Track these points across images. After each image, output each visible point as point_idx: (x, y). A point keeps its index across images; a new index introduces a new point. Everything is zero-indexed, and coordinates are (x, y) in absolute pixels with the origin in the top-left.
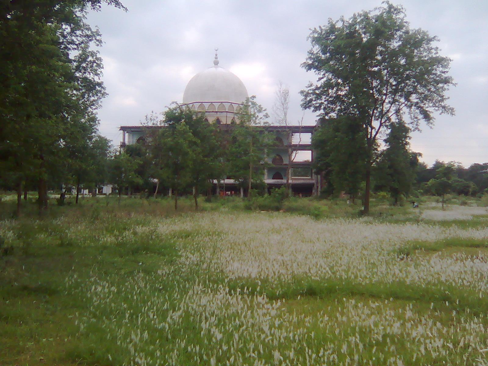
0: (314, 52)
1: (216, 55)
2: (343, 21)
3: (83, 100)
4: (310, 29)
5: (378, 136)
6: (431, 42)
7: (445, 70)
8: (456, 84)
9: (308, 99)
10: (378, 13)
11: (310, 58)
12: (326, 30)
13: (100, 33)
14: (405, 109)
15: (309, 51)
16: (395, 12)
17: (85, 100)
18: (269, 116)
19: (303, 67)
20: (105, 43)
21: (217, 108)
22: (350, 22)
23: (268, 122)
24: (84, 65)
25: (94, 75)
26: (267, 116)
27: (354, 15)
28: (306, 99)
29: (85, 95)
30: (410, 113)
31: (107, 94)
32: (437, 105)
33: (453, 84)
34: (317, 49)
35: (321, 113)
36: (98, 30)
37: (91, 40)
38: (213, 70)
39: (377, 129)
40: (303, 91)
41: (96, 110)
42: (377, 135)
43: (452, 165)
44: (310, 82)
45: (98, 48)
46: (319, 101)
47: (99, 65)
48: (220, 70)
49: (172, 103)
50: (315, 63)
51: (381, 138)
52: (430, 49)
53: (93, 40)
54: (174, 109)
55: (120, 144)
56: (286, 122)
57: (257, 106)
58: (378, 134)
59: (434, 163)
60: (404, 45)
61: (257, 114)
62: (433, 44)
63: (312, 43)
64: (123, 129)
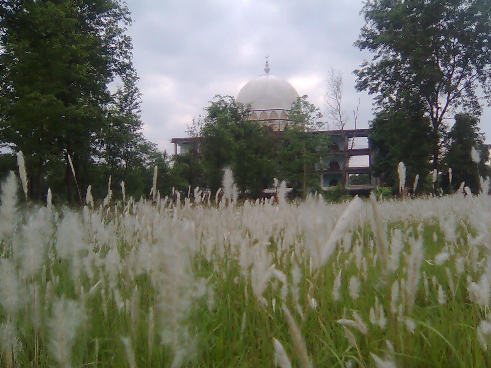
0: (368, 28)
1: (267, 62)
3: (126, 104)
4: (363, 2)
5: (445, 115)
9: (363, 79)
11: (364, 35)
13: (129, 11)
14: (476, 82)
18: (322, 116)
19: (356, 46)
20: (135, 21)
21: (269, 115)
23: (321, 122)
25: (124, 58)
26: (320, 115)
29: (127, 98)
31: (138, 78)
34: (372, 26)
35: (379, 96)
37: (119, 19)
38: (264, 78)
39: (443, 108)
40: (357, 70)
41: (140, 113)
42: (444, 114)
46: (376, 82)
47: (127, 46)
48: (272, 77)
49: (215, 97)
51: (449, 117)
56: (340, 113)
57: (309, 106)
58: (445, 113)
61: (310, 114)
63: (365, 18)
64: (175, 141)
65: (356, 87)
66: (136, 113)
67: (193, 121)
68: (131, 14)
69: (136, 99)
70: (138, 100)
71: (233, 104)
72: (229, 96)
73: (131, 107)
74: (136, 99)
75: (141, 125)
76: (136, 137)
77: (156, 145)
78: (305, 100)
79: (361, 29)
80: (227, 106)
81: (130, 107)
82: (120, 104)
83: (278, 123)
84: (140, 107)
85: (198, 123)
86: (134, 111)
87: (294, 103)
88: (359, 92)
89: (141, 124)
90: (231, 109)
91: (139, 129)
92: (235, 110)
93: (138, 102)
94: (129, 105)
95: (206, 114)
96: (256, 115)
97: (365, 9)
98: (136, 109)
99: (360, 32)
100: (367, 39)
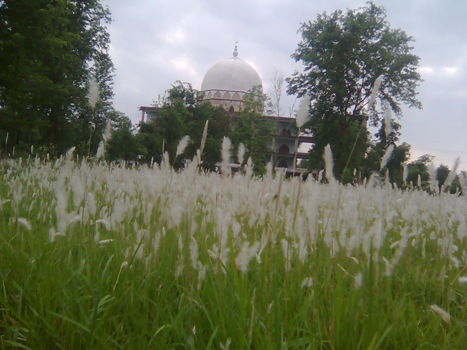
1: (236, 47)
2: (325, 16)
3: (101, 75)
4: (300, 23)
6: (408, 42)
7: (414, 67)
8: (423, 80)
9: (293, 86)
10: (361, 12)
11: (299, 50)
12: (314, 25)
13: (110, 12)
15: (299, 43)
16: (377, 12)
17: (103, 75)
19: (293, 57)
21: (232, 96)
22: (332, 17)
24: (94, 39)
27: (336, 11)
28: (290, 85)
30: (382, 104)
32: (407, 98)
33: (421, 80)
36: (108, 9)
37: (102, 18)
41: (112, 85)
43: (426, 158)
44: (296, 70)
45: (107, 25)
47: (106, 40)
48: (237, 61)
49: (176, 82)
50: (303, 54)
52: (407, 49)
53: (103, 18)
54: (178, 87)
55: (138, 123)
56: (278, 107)
59: (439, 166)
60: (382, 43)
62: (409, 44)
64: (143, 109)
65: (287, 91)
66: (109, 85)
67: (158, 96)
68: (111, 15)
69: (110, 72)
70: (111, 74)
71: (190, 90)
72: (188, 83)
73: (106, 79)
74: (110, 72)
75: (112, 96)
76: (107, 106)
77: (123, 114)
78: (259, 89)
79: (298, 44)
80: (185, 91)
81: (104, 79)
82: (96, 75)
83: (239, 104)
84: (113, 80)
85: (163, 98)
86: (107, 83)
87: (249, 91)
88: (289, 96)
89: (112, 94)
90: (188, 93)
91: (110, 99)
92: (191, 94)
93: (111, 75)
94: (104, 77)
95: (168, 95)
96: (220, 94)
97: (302, 29)
98: (109, 81)
99: (297, 47)
100: (301, 53)
